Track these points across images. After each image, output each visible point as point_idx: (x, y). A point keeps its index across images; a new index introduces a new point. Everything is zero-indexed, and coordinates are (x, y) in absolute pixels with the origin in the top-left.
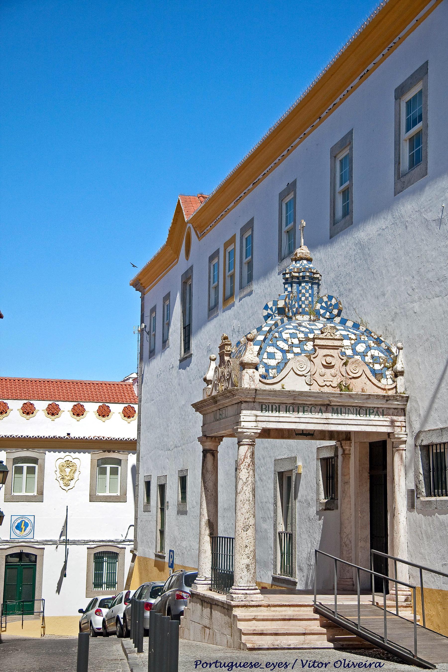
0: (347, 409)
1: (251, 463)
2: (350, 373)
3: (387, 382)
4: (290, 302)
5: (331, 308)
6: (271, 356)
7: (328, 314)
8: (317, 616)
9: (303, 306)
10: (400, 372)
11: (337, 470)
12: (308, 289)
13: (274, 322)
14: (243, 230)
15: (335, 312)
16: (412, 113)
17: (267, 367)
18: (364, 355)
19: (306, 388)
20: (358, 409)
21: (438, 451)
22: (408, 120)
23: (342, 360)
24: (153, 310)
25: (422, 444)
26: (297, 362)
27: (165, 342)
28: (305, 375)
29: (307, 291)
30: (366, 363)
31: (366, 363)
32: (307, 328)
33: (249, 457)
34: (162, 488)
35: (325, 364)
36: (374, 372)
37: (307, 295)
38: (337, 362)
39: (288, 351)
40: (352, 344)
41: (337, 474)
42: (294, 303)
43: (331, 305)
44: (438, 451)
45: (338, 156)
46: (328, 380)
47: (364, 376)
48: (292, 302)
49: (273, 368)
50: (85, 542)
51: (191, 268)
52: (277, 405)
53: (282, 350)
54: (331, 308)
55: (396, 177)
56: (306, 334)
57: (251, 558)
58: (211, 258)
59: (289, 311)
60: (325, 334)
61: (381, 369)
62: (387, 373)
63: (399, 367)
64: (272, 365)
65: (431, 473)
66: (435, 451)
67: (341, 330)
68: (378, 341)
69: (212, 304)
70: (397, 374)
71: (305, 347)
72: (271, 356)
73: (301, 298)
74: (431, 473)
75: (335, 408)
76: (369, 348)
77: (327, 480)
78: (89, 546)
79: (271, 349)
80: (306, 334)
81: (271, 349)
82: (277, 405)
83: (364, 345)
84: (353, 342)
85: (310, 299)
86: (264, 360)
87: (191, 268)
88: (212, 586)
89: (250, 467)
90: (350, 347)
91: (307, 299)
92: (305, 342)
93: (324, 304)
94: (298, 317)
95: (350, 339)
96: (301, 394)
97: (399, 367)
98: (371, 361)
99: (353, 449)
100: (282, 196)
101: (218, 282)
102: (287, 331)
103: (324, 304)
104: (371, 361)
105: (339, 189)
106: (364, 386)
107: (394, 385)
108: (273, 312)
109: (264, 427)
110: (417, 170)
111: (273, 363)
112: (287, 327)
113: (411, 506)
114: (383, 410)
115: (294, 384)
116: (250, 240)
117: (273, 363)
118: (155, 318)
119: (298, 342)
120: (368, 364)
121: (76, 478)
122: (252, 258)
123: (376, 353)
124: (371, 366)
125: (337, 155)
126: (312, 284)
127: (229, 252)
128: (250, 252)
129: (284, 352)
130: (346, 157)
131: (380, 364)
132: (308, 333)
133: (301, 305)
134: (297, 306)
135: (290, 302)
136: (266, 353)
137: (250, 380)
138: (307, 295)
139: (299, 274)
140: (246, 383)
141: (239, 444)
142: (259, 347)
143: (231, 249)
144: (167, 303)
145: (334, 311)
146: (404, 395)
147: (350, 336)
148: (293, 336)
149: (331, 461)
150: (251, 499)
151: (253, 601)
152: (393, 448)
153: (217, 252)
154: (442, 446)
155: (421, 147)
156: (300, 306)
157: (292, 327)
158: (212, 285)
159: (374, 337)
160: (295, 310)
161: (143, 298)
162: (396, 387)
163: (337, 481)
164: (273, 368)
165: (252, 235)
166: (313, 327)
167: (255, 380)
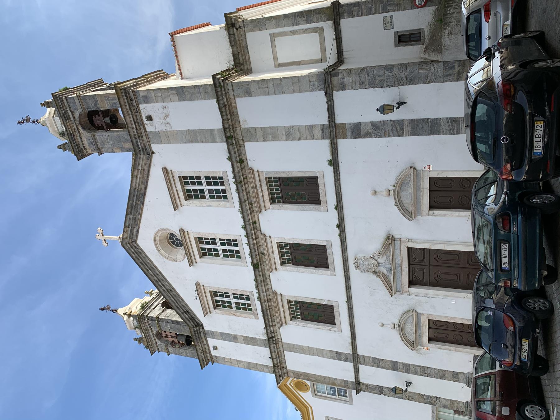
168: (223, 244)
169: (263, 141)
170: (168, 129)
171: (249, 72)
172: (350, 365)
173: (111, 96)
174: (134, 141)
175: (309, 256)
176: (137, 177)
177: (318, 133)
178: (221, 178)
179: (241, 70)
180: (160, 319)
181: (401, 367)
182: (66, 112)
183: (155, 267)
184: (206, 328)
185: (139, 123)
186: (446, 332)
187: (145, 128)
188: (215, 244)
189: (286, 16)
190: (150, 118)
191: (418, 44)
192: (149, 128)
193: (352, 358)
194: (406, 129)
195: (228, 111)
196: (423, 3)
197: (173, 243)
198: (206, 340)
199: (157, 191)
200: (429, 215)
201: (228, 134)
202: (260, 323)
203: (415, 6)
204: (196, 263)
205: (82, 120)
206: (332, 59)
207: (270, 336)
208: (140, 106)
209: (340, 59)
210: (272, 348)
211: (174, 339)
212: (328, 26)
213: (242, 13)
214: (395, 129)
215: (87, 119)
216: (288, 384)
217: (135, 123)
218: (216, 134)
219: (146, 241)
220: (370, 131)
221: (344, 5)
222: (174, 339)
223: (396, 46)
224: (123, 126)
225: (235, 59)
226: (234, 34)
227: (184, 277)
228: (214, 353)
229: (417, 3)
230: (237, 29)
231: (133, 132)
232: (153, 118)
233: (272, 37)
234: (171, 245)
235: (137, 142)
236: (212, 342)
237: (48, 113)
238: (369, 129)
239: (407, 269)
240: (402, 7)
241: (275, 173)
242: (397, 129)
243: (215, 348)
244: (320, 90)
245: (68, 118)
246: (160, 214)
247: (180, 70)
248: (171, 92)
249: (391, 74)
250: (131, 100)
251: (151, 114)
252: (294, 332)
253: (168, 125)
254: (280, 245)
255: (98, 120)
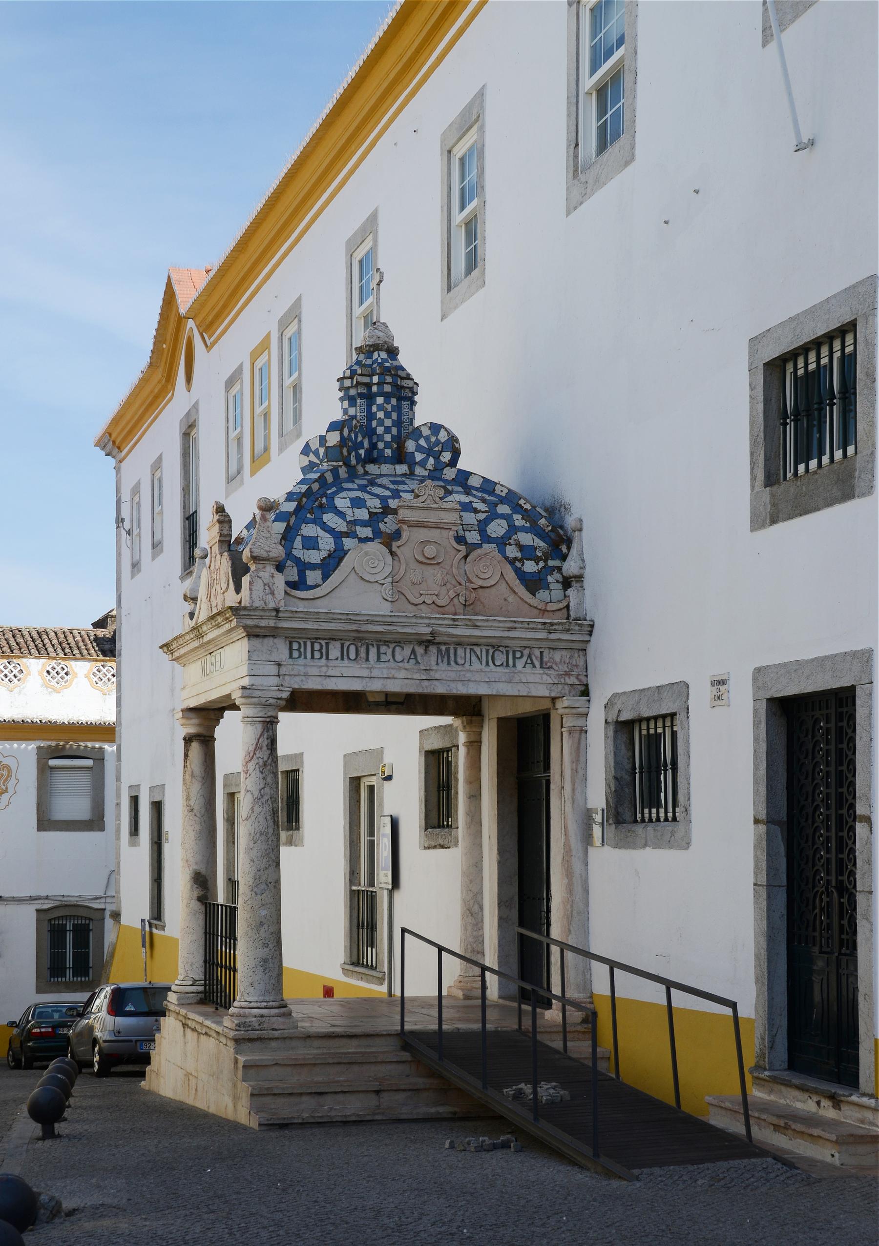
0: (468, 651)
1: (270, 761)
2: (474, 579)
4: (353, 435)
5: (436, 449)
6: (311, 543)
7: (431, 460)
8: (406, 1056)
9: (381, 445)
10: (575, 577)
11: (457, 773)
12: (390, 409)
13: (319, 475)
14: (284, 324)
15: (446, 457)
16: (603, 32)
17: (303, 567)
18: (502, 543)
20: (491, 651)
21: (652, 731)
22: (594, 49)
23: (460, 551)
24: (136, 490)
25: (621, 719)
27: (156, 546)
28: (382, 582)
29: (388, 415)
30: (506, 558)
31: (506, 558)
32: (388, 488)
33: (265, 748)
34: (157, 807)
35: (421, 558)
36: (521, 575)
37: (388, 423)
39: (347, 535)
40: (479, 521)
41: (457, 780)
42: (360, 439)
43: (438, 442)
44: (652, 731)
45: (454, 151)
46: (430, 592)
47: (503, 585)
48: (356, 437)
49: (313, 567)
50: (32, 899)
51: (196, 406)
52: (323, 643)
53: (330, 531)
54: (436, 449)
55: (571, 174)
56: (384, 499)
57: (271, 946)
58: (230, 383)
59: (349, 454)
60: (422, 499)
61: (539, 572)
62: (550, 579)
64: (313, 561)
65: (637, 775)
66: (644, 732)
67: (457, 492)
69: (233, 469)
71: (381, 525)
72: (311, 543)
73: (375, 428)
74: (637, 775)
75: (443, 648)
76: (513, 529)
77: (439, 791)
78: (39, 907)
79: (309, 530)
80: (384, 499)
81: (309, 530)
82: (323, 643)
83: (504, 523)
84: (482, 516)
85: (394, 431)
86: (294, 552)
87: (196, 406)
88: (205, 996)
89: (269, 767)
90: (476, 528)
91: (387, 430)
92: (380, 516)
93: (422, 442)
94: (372, 468)
95: (476, 511)
98: (519, 555)
100: (352, 245)
101: (242, 427)
102: (343, 494)
103: (422, 442)
104: (519, 555)
105: (458, 218)
107: (565, 603)
108: (318, 458)
109: (296, 686)
110: (614, 151)
111: (314, 557)
112: (345, 485)
114: (541, 653)
116: (295, 342)
117: (314, 557)
118: (139, 504)
119: (367, 517)
120: (512, 562)
121: (11, 791)
122: (300, 374)
123: (526, 539)
124: (518, 564)
125: (453, 147)
126: (400, 399)
127: (261, 369)
128: (296, 365)
129: (338, 536)
130: (471, 150)
131: (537, 560)
132: (389, 497)
133: (376, 444)
134: (366, 444)
135: (353, 435)
136: (299, 538)
138: (381, 415)
139: (371, 379)
142: (285, 524)
143: (263, 361)
144: (158, 475)
146: (585, 622)
147: (475, 505)
148: (357, 503)
149: (445, 755)
150: (271, 830)
151: (276, 1030)
152: (562, 727)
153: (239, 370)
154: (660, 723)
155: (620, 104)
156: (373, 446)
157: (356, 487)
158: (233, 435)
159: (525, 506)
160: (362, 452)
161: (118, 469)
162: (568, 607)
163: (457, 793)
164: (313, 567)
165: (299, 332)
166: (401, 487)
167: (276, 592)
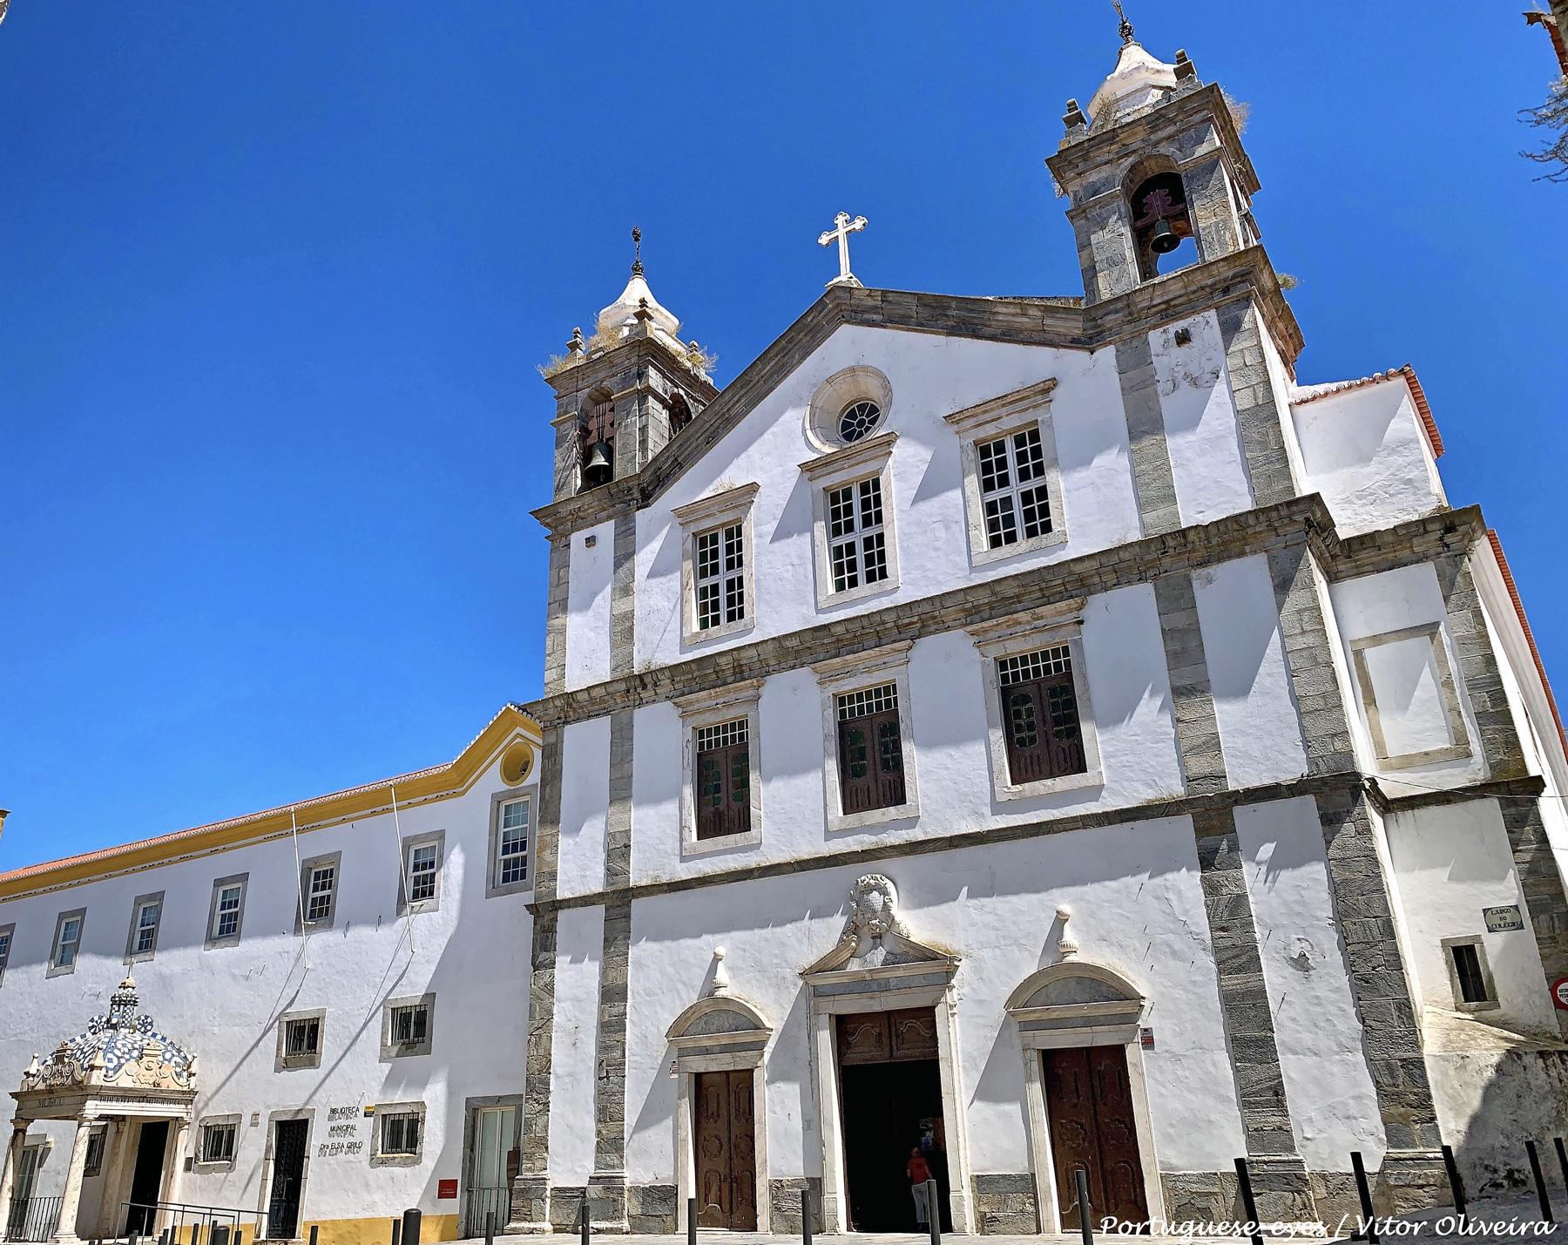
3: (183, 1081)
6: (110, 1060)
17: (108, 1069)
19: (131, 1085)
26: (131, 1066)
38: (154, 1066)
63: (193, 1070)
68: (179, 1051)
70: (191, 1075)
72: (110, 1060)
79: (110, 1055)
81: (110, 1055)
96: (130, 1089)
97: (193, 1070)
99: (126, 1128)
106: (169, 1084)
111: (111, 1066)
113: (188, 1168)
115: (124, 1082)
117: (111, 1066)
137: (96, 1079)
140: (94, 1081)
141: (80, 1126)
145: (145, 1025)
168: (868, 543)
169: (1163, 630)
170: (1160, 387)
171: (1332, 578)
172: (596, 885)
173: (1228, 235)
174: (1120, 305)
175: (870, 758)
176: (1023, 315)
177: (1199, 766)
178: (1047, 528)
179: (1334, 557)
180: (645, 398)
181: (615, 1011)
182: (1172, 121)
183: (786, 376)
184: (641, 517)
185: (1168, 312)
186: (724, 1112)
187: (1154, 327)
188: (867, 522)
189: (1491, 661)
190: (1183, 338)
191: (1456, 997)
192: (1155, 337)
193: (621, 886)
194: (1235, 982)
195: (1226, 539)
196: (1563, 1000)
197: (852, 415)
198: (609, 518)
199: (986, 368)
200: (1025, 1050)
201: (1170, 542)
202: (670, 655)
203: (1554, 982)
204: (810, 480)
205: (1153, 162)
206: (1392, 787)
207: (648, 680)
208: (1213, 312)
209: (1388, 807)
210: (616, 686)
211: (595, 433)
212: (1475, 770)
213: (1485, 541)
214: (1237, 952)
215: (1157, 171)
216: (519, 730)
217: (1167, 302)
218: (1162, 511)
219: (847, 347)
220: (1224, 891)
221: (1534, 803)
222: (595, 433)
223: (1444, 943)
224: (1147, 271)
225: (1361, 539)
226: (1426, 532)
227: (773, 454)
228: (577, 538)
229: (1561, 987)
230: (1441, 539)
231: (1142, 301)
232: (1185, 347)
233: (1431, 629)
234: (844, 410)
235: (1117, 312)
236: (606, 531)
237: (1159, 65)
238: (1229, 890)
239: (877, 1008)
240: (1547, 951)
241: (1082, 663)
242: (1237, 956)
243: (590, 541)
244: (1311, 761)
245: (1154, 130)
246: (935, 378)
247: (1314, 398)
248: (1260, 391)
249: (1376, 932)
250: (1226, 291)
251: (1196, 341)
252: (664, 736)
253: (1170, 385)
254: (890, 689)
255: (1157, 200)
